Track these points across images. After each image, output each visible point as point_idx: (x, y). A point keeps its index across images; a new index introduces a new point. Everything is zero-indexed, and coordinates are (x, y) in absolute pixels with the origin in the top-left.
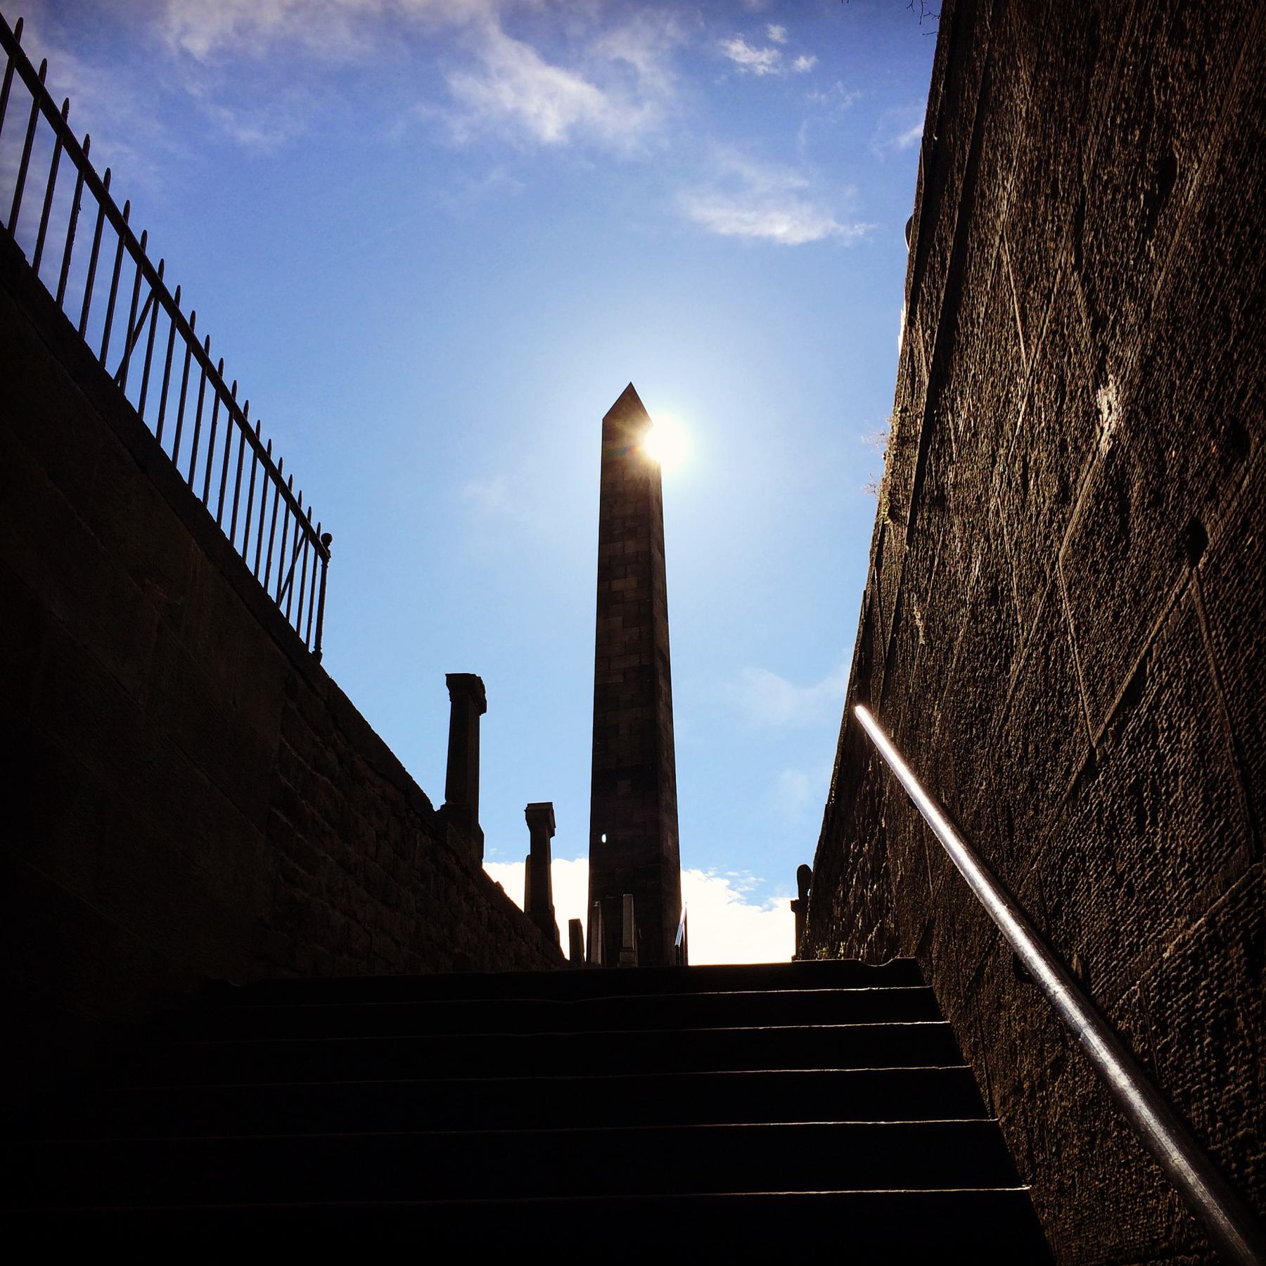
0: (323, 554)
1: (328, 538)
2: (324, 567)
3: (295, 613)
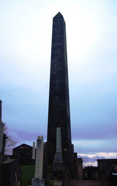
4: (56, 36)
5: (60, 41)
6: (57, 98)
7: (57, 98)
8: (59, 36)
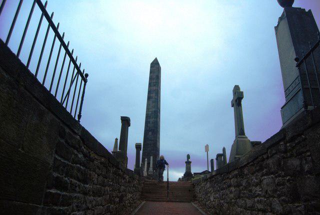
0: (86, 81)
1: (87, 75)
2: (85, 85)
3: (70, 107)
4: (152, 81)
5: (155, 85)
6: (150, 133)
7: (150, 133)
8: (154, 81)
